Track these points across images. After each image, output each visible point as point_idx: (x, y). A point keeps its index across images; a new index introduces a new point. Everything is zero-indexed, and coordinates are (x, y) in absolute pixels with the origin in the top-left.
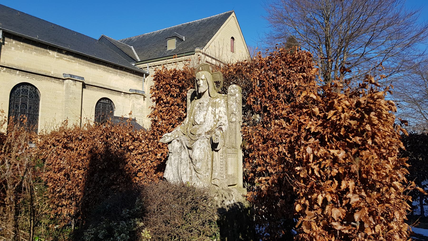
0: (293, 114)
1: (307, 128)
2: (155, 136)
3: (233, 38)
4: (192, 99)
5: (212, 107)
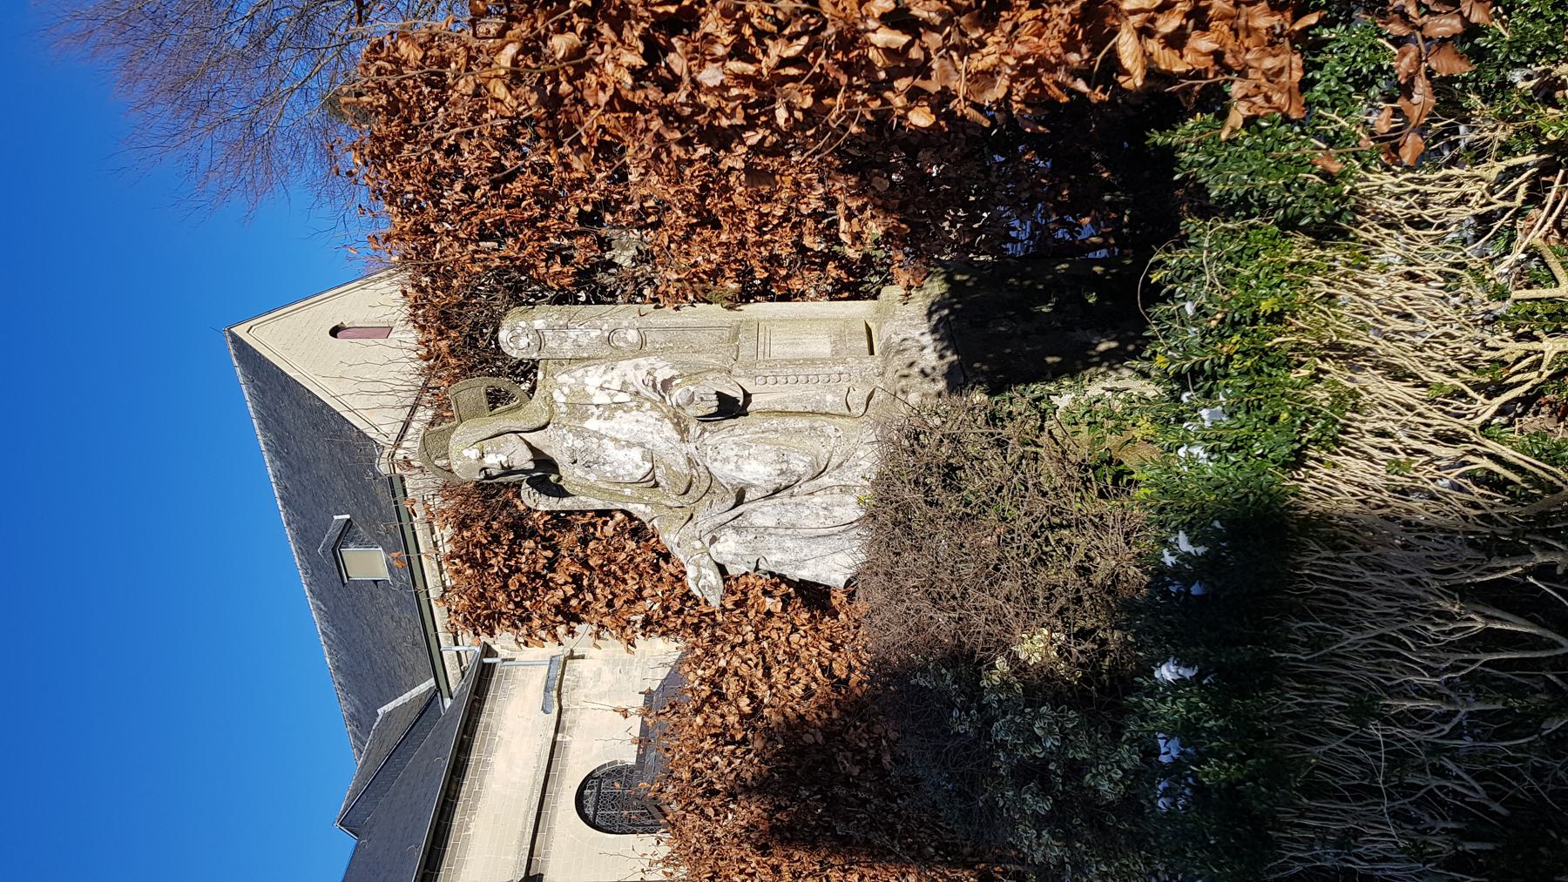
0: (581, 130)
1: (628, 80)
2: (701, 621)
3: (334, 332)
4: (561, 493)
5: (585, 417)
